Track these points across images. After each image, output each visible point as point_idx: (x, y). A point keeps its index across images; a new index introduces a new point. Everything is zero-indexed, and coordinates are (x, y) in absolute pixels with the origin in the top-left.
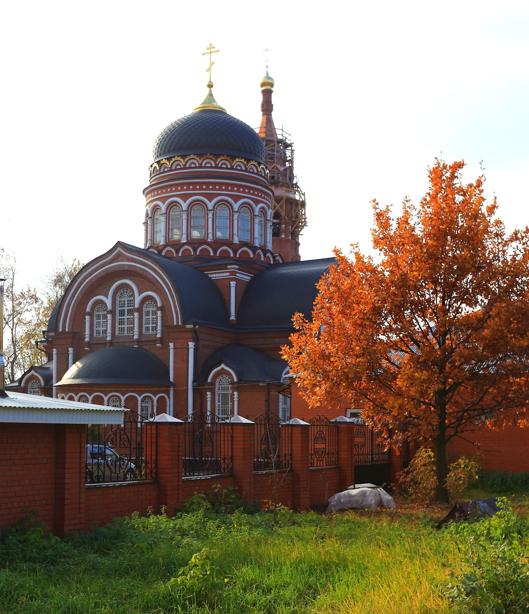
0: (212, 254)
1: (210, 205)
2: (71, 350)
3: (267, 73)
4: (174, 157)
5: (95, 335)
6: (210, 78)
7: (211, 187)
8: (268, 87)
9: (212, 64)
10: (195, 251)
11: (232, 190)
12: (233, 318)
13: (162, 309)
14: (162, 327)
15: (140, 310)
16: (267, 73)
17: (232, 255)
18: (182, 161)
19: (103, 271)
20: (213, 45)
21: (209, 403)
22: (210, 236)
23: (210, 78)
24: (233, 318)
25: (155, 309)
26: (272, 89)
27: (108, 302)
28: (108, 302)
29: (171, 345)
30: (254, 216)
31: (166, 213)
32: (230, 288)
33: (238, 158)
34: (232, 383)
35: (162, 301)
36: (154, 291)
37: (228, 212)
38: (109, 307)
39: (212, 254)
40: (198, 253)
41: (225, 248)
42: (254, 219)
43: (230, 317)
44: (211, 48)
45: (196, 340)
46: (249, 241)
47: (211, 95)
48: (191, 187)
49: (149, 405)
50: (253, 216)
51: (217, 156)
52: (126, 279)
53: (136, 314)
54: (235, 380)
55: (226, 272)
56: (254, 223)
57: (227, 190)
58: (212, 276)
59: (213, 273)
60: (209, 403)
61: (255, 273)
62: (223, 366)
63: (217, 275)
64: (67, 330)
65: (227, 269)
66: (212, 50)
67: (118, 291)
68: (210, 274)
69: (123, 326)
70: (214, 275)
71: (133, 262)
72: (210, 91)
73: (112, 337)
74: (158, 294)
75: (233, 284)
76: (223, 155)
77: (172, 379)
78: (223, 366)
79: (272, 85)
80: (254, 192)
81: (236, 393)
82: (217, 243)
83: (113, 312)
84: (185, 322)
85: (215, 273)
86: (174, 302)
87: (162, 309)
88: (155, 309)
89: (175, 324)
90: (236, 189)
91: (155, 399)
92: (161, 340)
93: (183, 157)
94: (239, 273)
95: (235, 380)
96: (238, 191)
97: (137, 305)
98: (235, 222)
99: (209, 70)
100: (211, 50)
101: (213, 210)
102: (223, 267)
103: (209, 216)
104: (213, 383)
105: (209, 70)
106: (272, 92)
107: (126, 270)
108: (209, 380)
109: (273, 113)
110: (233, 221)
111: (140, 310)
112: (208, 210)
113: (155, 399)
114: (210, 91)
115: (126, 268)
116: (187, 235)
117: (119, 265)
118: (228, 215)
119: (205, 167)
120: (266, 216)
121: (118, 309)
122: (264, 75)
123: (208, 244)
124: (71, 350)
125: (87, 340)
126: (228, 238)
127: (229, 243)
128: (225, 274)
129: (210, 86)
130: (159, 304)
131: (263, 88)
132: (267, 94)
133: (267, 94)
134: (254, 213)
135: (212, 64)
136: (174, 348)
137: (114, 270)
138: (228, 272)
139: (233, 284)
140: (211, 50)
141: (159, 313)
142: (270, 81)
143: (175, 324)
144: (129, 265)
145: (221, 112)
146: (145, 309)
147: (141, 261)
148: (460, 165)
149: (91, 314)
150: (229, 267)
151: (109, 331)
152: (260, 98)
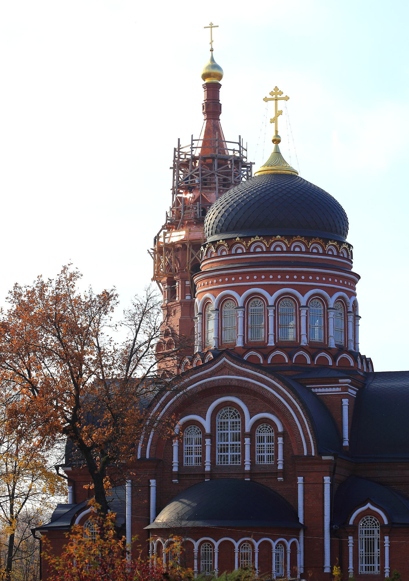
0: (309, 362)
1: (303, 300)
2: (153, 482)
3: (212, 60)
4: (254, 237)
5: (185, 463)
6: (277, 132)
7: (263, 277)
8: (215, 80)
9: (279, 113)
10: (290, 358)
11: (327, 282)
12: (346, 443)
13: (284, 435)
14: (284, 457)
15: (251, 435)
16: (212, 60)
17: (331, 363)
18: (266, 243)
19: (201, 385)
20: (280, 88)
21: (351, 550)
22: (304, 338)
23: (277, 132)
24: (346, 443)
25: (272, 434)
26: (220, 82)
27: (206, 424)
28: (206, 424)
29: (300, 479)
30: (328, 309)
31: (244, 307)
32: (342, 406)
33: (296, 236)
34: (383, 526)
35: (283, 426)
36: (272, 413)
37: (322, 308)
38: (208, 430)
39: (309, 362)
40: (269, 362)
41: (323, 354)
42: (327, 313)
43: (342, 442)
44: (276, 94)
45: (332, 475)
46: (343, 344)
47: (277, 152)
48: (287, 277)
49: (249, 551)
50: (327, 309)
51: (309, 238)
52: (231, 396)
53: (247, 440)
54: (386, 522)
55: (336, 387)
56: (347, 322)
57: (321, 281)
58: (316, 390)
59: (318, 388)
60: (351, 550)
61: (360, 386)
62: (369, 505)
63: (323, 390)
64: (148, 457)
65: (339, 383)
66: (279, 96)
67: (219, 410)
68: (315, 388)
69: (226, 454)
70: (320, 390)
71: (244, 376)
72: (277, 148)
73: (211, 467)
74: (278, 417)
75: (345, 401)
76: (315, 238)
77: (301, 521)
78: (369, 505)
79: (220, 77)
80: (339, 281)
81: (387, 538)
82: (314, 348)
83: (212, 436)
84: (320, 453)
85: (321, 388)
86: (304, 428)
87: (284, 435)
88: (272, 434)
89: (305, 454)
90: (287, 277)
91: (256, 545)
92: (283, 473)
93: (267, 237)
94: (351, 388)
95: (386, 522)
96: (333, 282)
97: (247, 429)
98: (331, 321)
99: (274, 121)
100: (276, 95)
101: (274, 306)
102: (334, 381)
103: (302, 314)
104: (355, 526)
105: (274, 121)
106: (219, 86)
107: (235, 386)
108: (351, 522)
109: (221, 117)
110: (328, 319)
111: (251, 435)
112: (300, 307)
113: (256, 545)
114: (277, 148)
115: (234, 383)
116: (275, 336)
117: (223, 379)
118: (322, 313)
119: (255, 253)
120: (347, 307)
121: (218, 432)
122: (208, 62)
123: (303, 348)
124: (153, 482)
125: (175, 469)
126: (323, 341)
127: (323, 347)
128: (334, 390)
129: (277, 141)
130: (280, 429)
131: (207, 81)
132: (213, 90)
133: (213, 90)
134: (347, 309)
135: (279, 113)
136: (304, 484)
137: (216, 384)
138: (339, 387)
139: (345, 401)
140: (276, 95)
141: (280, 440)
142: (216, 71)
143: (305, 454)
144: (238, 380)
145: (292, 177)
146: (257, 435)
147: (257, 376)
148: (287, 98)
149: (179, 437)
150: (340, 381)
151: (208, 459)
152: (201, 96)
